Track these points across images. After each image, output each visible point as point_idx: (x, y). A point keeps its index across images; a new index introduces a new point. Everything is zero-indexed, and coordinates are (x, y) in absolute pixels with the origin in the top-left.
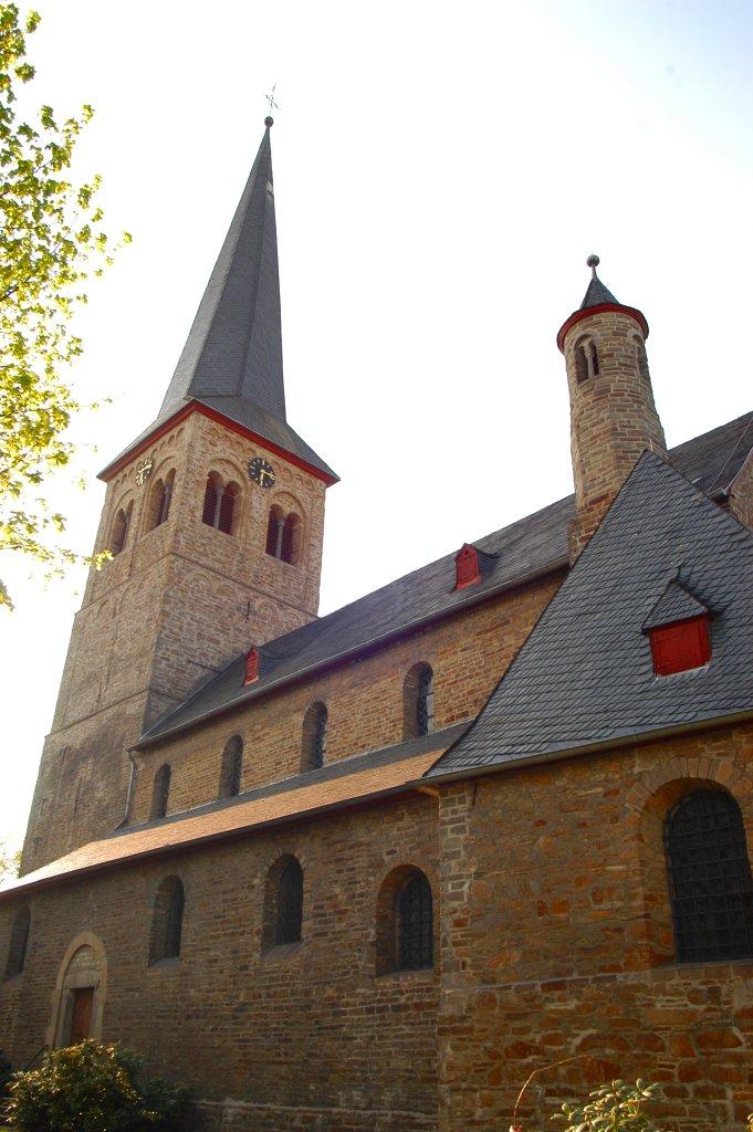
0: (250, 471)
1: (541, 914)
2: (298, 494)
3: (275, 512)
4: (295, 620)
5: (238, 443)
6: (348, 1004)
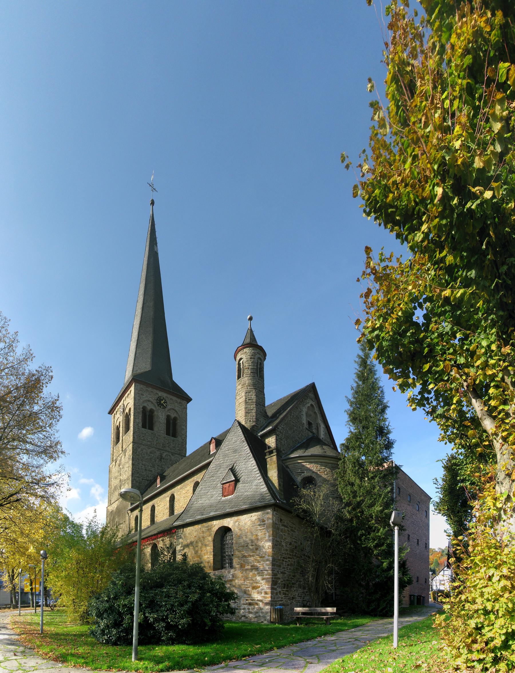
0: (157, 403)
2: (177, 409)
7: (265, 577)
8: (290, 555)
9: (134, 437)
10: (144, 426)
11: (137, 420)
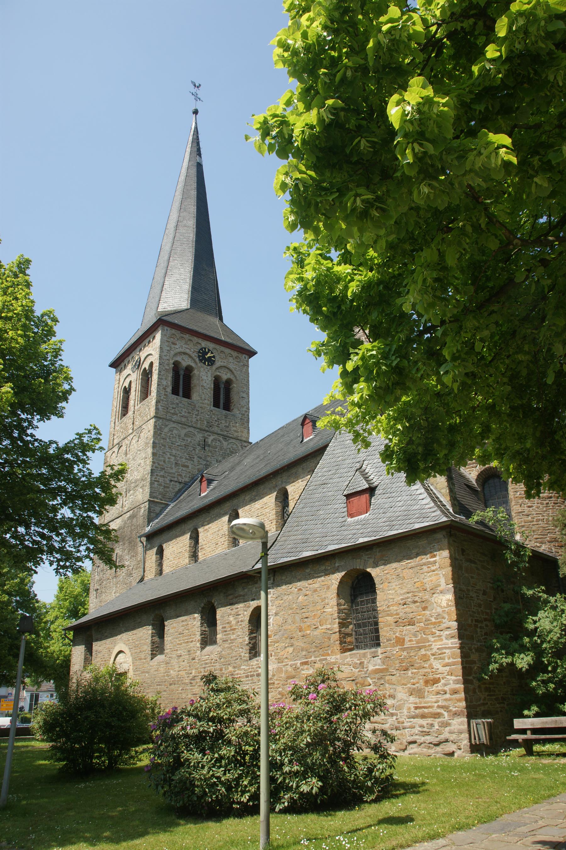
0: (199, 356)
1: (300, 631)
2: (231, 366)
3: (217, 381)
4: (235, 446)
5: (190, 340)
6: (238, 674)
7: (447, 661)
8: (487, 613)
9: (157, 409)
10: (175, 391)
11: (164, 383)
